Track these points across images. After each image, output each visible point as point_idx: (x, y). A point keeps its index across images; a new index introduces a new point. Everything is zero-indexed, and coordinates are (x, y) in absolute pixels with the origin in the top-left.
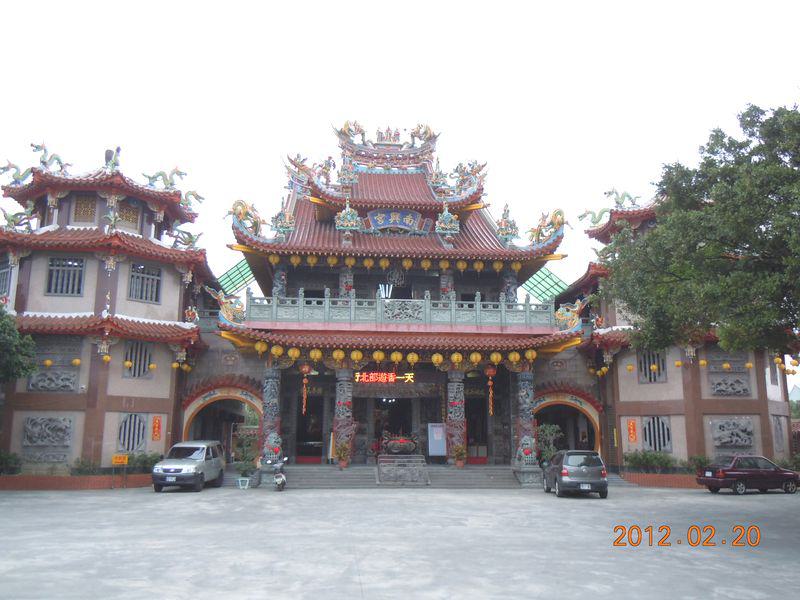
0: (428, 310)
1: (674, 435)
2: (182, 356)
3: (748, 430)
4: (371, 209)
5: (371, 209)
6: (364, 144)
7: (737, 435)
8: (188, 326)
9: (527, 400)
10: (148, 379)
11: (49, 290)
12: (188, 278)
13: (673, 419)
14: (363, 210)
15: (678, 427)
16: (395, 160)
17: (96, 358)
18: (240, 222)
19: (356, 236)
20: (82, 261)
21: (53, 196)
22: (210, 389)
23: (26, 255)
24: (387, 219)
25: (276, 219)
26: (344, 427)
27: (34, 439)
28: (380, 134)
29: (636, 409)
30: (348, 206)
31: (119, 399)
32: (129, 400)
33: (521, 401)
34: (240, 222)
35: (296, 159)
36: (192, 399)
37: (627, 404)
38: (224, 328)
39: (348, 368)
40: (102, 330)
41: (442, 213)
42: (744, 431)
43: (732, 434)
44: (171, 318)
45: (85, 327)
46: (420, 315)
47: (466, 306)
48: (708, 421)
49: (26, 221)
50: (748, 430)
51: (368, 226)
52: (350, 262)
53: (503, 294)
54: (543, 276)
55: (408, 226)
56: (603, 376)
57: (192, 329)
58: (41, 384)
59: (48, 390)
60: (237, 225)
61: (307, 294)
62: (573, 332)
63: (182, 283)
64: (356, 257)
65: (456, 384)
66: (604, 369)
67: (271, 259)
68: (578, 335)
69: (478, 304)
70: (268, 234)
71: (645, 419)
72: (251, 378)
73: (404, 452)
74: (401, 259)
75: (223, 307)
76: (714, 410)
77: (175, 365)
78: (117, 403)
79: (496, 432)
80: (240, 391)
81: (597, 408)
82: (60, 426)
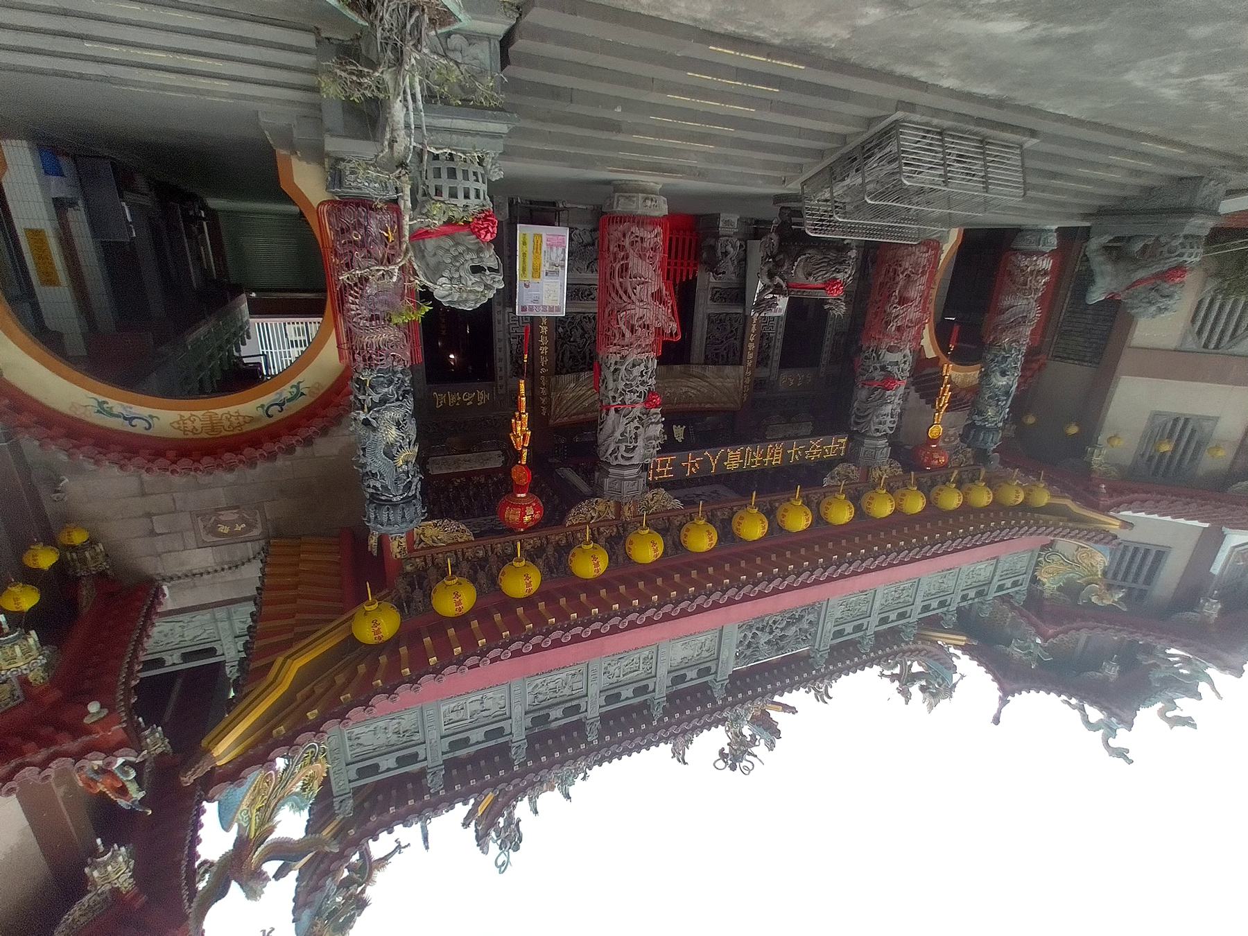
9: (393, 434)
47: (627, 692)
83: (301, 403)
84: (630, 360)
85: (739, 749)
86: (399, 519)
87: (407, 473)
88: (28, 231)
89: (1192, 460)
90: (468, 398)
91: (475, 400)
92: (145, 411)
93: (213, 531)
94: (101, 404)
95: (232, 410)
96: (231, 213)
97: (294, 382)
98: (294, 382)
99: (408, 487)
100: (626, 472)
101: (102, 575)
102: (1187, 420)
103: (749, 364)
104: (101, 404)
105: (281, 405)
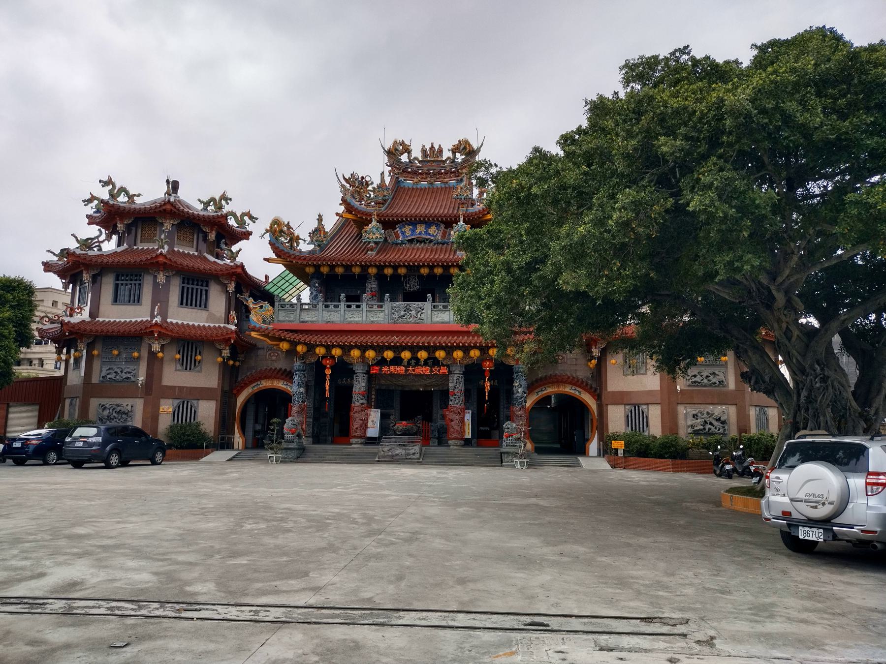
0: (429, 312)
1: (651, 423)
2: (226, 353)
3: (722, 419)
4: (398, 222)
5: (398, 222)
6: (410, 161)
7: (711, 424)
9: (520, 390)
10: (199, 371)
11: (182, 304)
12: (232, 287)
13: (651, 407)
14: (388, 224)
15: (655, 414)
16: (438, 175)
18: (276, 238)
20: (140, 276)
21: (122, 222)
22: (255, 380)
23: (96, 272)
24: (413, 231)
25: (313, 234)
26: (359, 412)
27: (104, 420)
28: (424, 151)
29: (621, 398)
30: (461, 220)
31: (173, 388)
33: (515, 391)
34: (276, 238)
35: (350, 179)
36: (243, 388)
37: (613, 393)
38: (254, 329)
40: (152, 333)
41: (457, 224)
42: (718, 420)
43: (706, 422)
44: (218, 321)
45: (138, 329)
46: (423, 316)
48: (682, 410)
49: (98, 244)
50: (722, 419)
51: (398, 237)
55: (432, 236)
58: (109, 376)
59: (115, 381)
60: (274, 241)
61: (349, 299)
64: (361, 266)
65: (456, 375)
67: (307, 270)
69: (364, 306)
70: (305, 247)
71: (627, 407)
72: (283, 369)
73: (406, 433)
74: (419, 267)
75: (253, 312)
76: (687, 398)
77: (220, 359)
78: (171, 392)
80: (282, 382)
82: (123, 410)
83: (536, 391)
84: (459, 404)
85: (360, 189)
92: (572, 391)
95: (553, 390)
96: (554, 443)
99: (517, 376)
102: (186, 369)
103: (373, 389)
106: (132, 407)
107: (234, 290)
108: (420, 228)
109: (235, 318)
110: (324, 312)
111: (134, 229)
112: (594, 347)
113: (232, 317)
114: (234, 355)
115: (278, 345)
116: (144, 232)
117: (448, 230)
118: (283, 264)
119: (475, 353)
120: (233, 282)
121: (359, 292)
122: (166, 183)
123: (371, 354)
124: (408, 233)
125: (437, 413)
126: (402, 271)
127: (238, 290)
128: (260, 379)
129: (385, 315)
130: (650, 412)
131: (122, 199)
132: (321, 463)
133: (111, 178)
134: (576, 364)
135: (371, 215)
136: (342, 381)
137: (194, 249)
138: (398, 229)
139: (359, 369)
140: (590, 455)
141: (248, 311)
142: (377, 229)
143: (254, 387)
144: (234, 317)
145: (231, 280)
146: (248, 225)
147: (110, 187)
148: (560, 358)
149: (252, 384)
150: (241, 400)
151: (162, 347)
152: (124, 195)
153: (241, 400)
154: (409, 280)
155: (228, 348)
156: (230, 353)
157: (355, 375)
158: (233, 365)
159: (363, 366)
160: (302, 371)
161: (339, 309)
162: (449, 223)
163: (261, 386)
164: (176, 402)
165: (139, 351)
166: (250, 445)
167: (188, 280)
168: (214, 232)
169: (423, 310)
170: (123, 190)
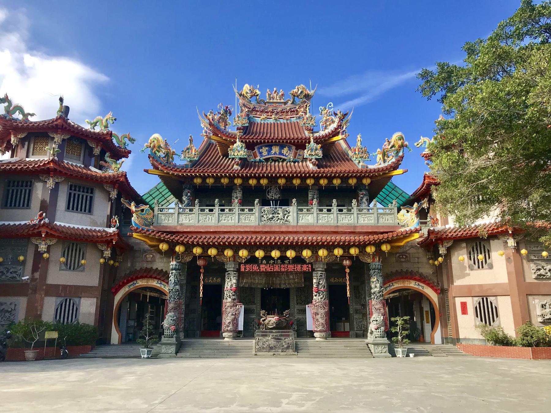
2: (108, 253)
4: (257, 144)
5: (257, 144)
8: (111, 230)
10: (82, 271)
11: (68, 208)
12: (114, 194)
17: (38, 255)
19: (244, 162)
21: (15, 136)
22: (132, 280)
24: (269, 152)
29: (469, 291)
32: (65, 287)
39: (234, 261)
47: (325, 210)
52: (238, 181)
53: (354, 201)
54: (390, 190)
56: (440, 265)
57: (114, 232)
62: (413, 229)
63: (110, 199)
65: (319, 272)
66: (440, 259)
68: (417, 231)
69: (335, 209)
72: (164, 271)
77: (102, 260)
79: (357, 311)
80: (156, 281)
81: (436, 291)
86: (377, 266)
87: (374, 276)
88: (292, 395)
89: (65, 251)
90: (336, 280)
91: (335, 279)
93: (406, 256)
94: (423, 289)
95: (400, 285)
97: (386, 291)
98: (386, 291)
99: (374, 272)
100: (321, 269)
101: (428, 252)
104: (423, 289)
105: (390, 286)
106: (15, 305)
107: (116, 197)
108: (275, 150)
109: (117, 221)
110: (200, 215)
111: (27, 143)
112: (441, 246)
113: (114, 221)
114: (113, 257)
115: (158, 246)
116: (36, 146)
117: (298, 151)
118: (159, 175)
119: (338, 252)
120: (115, 190)
121: (223, 202)
122: (59, 101)
123: (243, 253)
124: (265, 153)
125: (294, 306)
126: (264, 182)
127: (119, 196)
128: (137, 278)
129: (255, 218)
130: (499, 302)
131: (18, 116)
132: (200, 357)
133: (7, 97)
134: (418, 263)
135: (235, 138)
136: (208, 280)
137: (82, 162)
138: (256, 150)
139: (230, 267)
140: (435, 343)
141: (129, 213)
142: (241, 148)
143: (131, 285)
144: (116, 221)
145: (114, 188)
146: (128, 145)
147: (6, 104)
148: (404, 257)
149: (129, 283)
150: (118, 297)
151: (49, 247)
152: (19, 112)
153: (118, 297)
154: (271, 189)
155: (109, 249)
156: (111, 254)
157: (227, 273)
158: (113, 265)
159: (235, 264)
160: (178, 269)
161: (214, 212)
162: (301, 145)
163: (137, 285)
164: (59, 300)
165: (25, 256)
166: (124, 341)
167: (75, 187)
168: (99, 147)
169: (289, 213)
170: (20, 109)
